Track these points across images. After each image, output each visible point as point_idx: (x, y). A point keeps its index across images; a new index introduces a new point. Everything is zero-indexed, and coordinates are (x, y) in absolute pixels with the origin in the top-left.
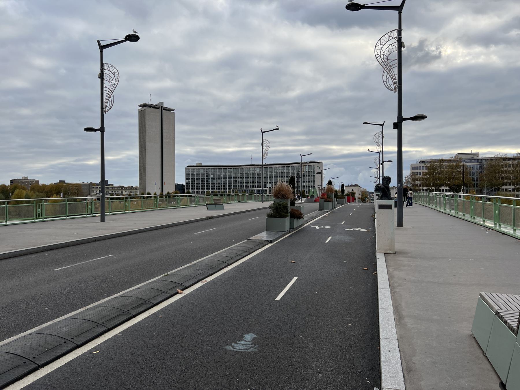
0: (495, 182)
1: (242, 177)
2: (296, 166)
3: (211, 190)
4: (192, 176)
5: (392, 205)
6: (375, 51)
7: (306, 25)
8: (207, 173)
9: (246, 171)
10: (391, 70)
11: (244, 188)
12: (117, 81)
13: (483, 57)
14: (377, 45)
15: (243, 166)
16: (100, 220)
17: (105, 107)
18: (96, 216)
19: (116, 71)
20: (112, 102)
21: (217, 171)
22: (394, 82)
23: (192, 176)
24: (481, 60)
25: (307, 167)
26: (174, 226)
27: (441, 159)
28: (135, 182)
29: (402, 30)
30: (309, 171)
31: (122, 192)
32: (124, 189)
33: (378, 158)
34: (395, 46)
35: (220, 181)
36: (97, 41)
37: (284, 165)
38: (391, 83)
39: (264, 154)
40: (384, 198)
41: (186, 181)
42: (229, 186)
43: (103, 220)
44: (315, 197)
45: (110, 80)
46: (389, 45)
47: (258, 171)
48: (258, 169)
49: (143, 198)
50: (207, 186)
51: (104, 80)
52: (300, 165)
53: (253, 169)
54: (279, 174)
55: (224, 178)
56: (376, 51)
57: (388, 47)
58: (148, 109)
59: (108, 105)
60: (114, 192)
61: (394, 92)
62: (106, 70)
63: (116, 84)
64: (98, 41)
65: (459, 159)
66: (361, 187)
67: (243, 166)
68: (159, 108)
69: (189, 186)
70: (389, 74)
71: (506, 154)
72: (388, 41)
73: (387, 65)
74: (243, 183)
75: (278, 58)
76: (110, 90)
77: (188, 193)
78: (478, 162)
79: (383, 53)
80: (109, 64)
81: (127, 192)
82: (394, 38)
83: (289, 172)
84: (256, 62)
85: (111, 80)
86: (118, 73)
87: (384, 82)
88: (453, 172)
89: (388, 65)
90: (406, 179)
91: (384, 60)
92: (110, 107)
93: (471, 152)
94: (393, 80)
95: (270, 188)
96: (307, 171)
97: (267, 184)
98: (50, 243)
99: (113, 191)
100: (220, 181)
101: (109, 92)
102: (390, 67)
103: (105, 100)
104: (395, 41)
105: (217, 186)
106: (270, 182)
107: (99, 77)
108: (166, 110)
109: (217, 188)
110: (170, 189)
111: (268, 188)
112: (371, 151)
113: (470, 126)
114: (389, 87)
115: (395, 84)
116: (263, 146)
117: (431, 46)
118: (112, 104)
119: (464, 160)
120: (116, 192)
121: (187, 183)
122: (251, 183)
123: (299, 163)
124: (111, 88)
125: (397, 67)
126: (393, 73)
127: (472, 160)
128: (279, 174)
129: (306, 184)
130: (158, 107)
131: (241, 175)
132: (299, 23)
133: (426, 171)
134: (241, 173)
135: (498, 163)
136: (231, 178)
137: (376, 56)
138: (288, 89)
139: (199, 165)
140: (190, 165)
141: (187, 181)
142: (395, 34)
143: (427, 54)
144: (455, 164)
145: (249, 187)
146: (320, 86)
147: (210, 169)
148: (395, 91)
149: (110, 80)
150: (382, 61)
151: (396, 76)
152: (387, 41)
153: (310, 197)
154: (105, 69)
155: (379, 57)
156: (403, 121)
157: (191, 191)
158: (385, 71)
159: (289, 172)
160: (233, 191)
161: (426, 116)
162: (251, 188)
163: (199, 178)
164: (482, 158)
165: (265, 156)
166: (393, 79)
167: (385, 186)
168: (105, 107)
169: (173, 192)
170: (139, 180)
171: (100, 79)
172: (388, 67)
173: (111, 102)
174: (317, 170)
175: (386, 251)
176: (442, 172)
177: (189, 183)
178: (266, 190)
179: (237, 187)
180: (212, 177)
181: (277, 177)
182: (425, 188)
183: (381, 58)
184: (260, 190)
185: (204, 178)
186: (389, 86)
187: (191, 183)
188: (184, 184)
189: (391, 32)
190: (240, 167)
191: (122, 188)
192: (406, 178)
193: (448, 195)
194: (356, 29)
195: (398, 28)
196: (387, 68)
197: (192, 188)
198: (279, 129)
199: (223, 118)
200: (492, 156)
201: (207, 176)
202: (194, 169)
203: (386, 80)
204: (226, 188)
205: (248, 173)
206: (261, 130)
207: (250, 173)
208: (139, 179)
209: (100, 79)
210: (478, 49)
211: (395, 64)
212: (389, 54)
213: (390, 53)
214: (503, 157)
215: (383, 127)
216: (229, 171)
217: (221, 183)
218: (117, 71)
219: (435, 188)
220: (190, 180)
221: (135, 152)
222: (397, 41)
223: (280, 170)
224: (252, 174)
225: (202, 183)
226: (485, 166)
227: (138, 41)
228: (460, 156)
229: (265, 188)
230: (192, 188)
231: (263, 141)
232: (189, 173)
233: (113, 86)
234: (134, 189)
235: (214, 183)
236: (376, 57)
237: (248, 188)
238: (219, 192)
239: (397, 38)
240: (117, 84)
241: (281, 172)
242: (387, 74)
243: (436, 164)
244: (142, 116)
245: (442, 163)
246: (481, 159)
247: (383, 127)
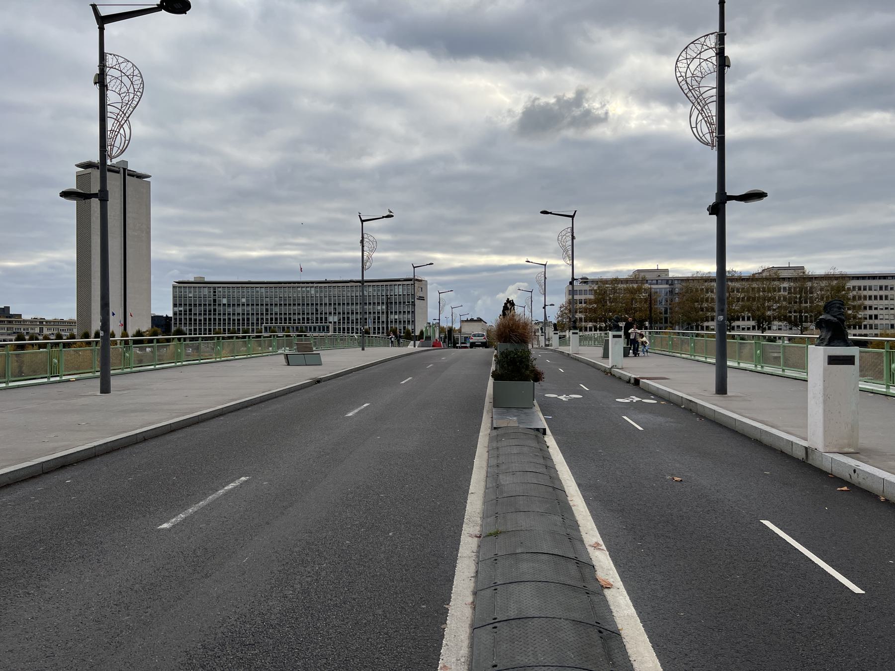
0: (693, 315)
1: (282, 303)
2: (381, 285)
4: (185, 300)
5: (854, 356)
6: (676, 70)
7: (394, 48)
10: (706, 107)
12: (139, 94)
13: (667, 121)
14: (680, 59)
16: (99, 389)
17: (109, 147)
18: (69, 381)
19: (136, 72)
20: (127, 138)
21: (234, 292)
22: (711, 130)
23: (185, 300)
24: (665, 126)
25: (401, 287)
27: (615, 279)
28: (67, 310)
29: (725, 34)
30: (403, 295)
31: (41, 330)
32: (44, 325)
33: (543, 273)
34: (712, 63)
35: (239, 310)
36: (91, 5)
38: (705, 130)
39: (365, 262)
40: (836, 342)
42: (258, 320)
43: (105, 389)
44: (433, 340)
45: (123, 91)
46: (702, 60)
47: (313, 292)
48: (313, 289)
49: (157, 343)
50: (215, 319)
51: (107, 90)
52: (412, 282)
53: (304, 289)
54: (352, 299)
55: (249, 305)
56: (677, 71)
57: (700, 63)
59: (117, 144)
60: (24, 330)
61: (710, 147)
62: (112, 67)
63: (137, 100)
64: (94, 7)
65: (642, 278)
66: (486, 323)
68: (118, 172)
69: (189, 318)
70: (702, 114)
71: (709, 273)
72: (700, 53)
73: (698, 97)
74: (285, 314)
75: (345, 99)
76: (121, 113)
77: (179, 332)
78: (667, 284)
79: (691, 75)
80: (118, 56)
81: (52, 329)
82: (712, 48)
83: (369, 296)
84: (305, 103)
85: (124, 90)
86: (141, 77)
87: (692, 128)
88: (633, 299)
89: (701, 97)
90: (562, 309)
91: (692, 87)
92: (121, 148)
94: (708, 124)
95: (335, 323)
96: (400, 294)
97: (330, 317)
98: (55, 450)
99: (22, 327)
100: (239, 310)
101: (119, 117)
102: (703, 102)
103: (109, 132)
104: (712, 53)
105: (234, 320)
106: (335, 313)
107: (95, 83)
108: (132, 176)
109: (234, 324)
110: (140, 323)
111: (331, 323)
112: (532, 262)
113: (647, 228)
114: (701, 138)
115: (712, 132)
116: (363, 246)
117: (594, 101)
118: (127, 142)
119: (647, 280)
120: (28, 329)
121: (177, 314)
122: (200, 314)
123: (410, 280)
124: (124, 108)
125: (716, 101)
126: (709, 112)
127: (659, 281)
128: (352, 299)
129: (409, 317)
130: (117, 169)
131: (280, 300)
132: (382, 43)
133: (592, 297)
134: (281, 296)
135: (696, 285)
136: (200, 305)
137: (677, 79)
138: (362, 152)
139: (198, 280)
140: (181, 280)
141: (176, 309)
142: (712, 41)
143: (588, 113)
144: (635, 286)
146: (416, 152)
147: (308, 287)
148: (713, 146)
149: (123, 91)
150: (689, 88)
151: (714, 118)
152: (699, 52)
153: (425, 340)
154: (110, 66)
155: (684, 82)
156: (727, 202)
157: (183, 328)
158: (694, 107)
159: (369, 296)
160: (266, 328)
161: (767, 193)
162: (300, 323)
163: (200, 305)
164: (674, 278)
165: (368, 264)
166: (709, 124)
168: (109, 147)
169: (147, 331)
170: (77, 307)
171: (96, 88)
172: (699, 101)
173: (125, 138)
174: (419, 294)
175: (842, 448)
176: (614, 300)
177: (180, 314)
178: (328, 327)
179: (274, 322)
180: (224, 303)
181: (348, 304)
182: (590, 325)
183: (687, 83)
184: (316, 327)
185: (210, 305)
186: (701, 135)
187: (184, 314)
188: (171, 314)
189: (706, 36)
190: (280, 285)
191: (42, 322)
192: (561, 308)
194: (476, 62)
195: (718, 31)
196: (698, 103)
197: (185, 324)
198: (392, 216)
199: (243, 196)
200: (689, 275)
201: (215, 301)
203: (697, 124)
204: (253, 323)
205: (294, 296)
206: (360, 216)
207: (298, 297)
208: (77, 305)
209: (98, 87)
210: (660, 109)
211: (713, 96)
212: (702, 78)
213: (703, 76)
214: (706, 277)
215: (573, 220)
216: (257, 292)
217: (344, 313)
218: (138, 72)
219: (606, 324)
220: (182, 309)
221: (71, 254)
222: (717, 54)
223: (353, 291)
224: (301, 298)
225: (205, 314)
226: (677, 291)
227: (186, 13)
228: (642, 274)
229: (327, 323)
230: (185, 324)
231: (363, 237)
233: (129, 103)
234: (66, 324)
235: (229, 314)
236: (678, 82)
237: (294, 323)
238: (253, 331)
239: (716, 48)
240: (139, 100)
241: (356, 296)
242: (699, 114)
243: (607, 286)
245: (616, 285)
246: (672, 279)
247: (574, 220)
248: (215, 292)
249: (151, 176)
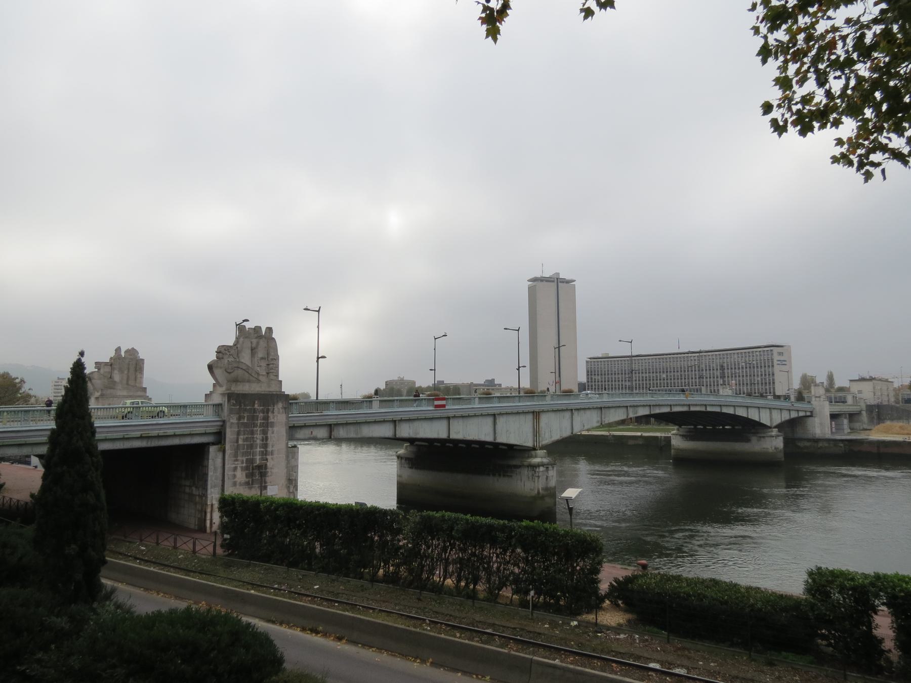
15: (666, 355)
26: (469, 416)
37: (726, 352)
58: (539, 284)
67: (666, 355)
68: (553, 281)
93: (630, 354)
108: (563, 282)
129: (758, 379)
139: (604, 356)
202: (727, 354)
209: (769, 43)
244: (532, 292)
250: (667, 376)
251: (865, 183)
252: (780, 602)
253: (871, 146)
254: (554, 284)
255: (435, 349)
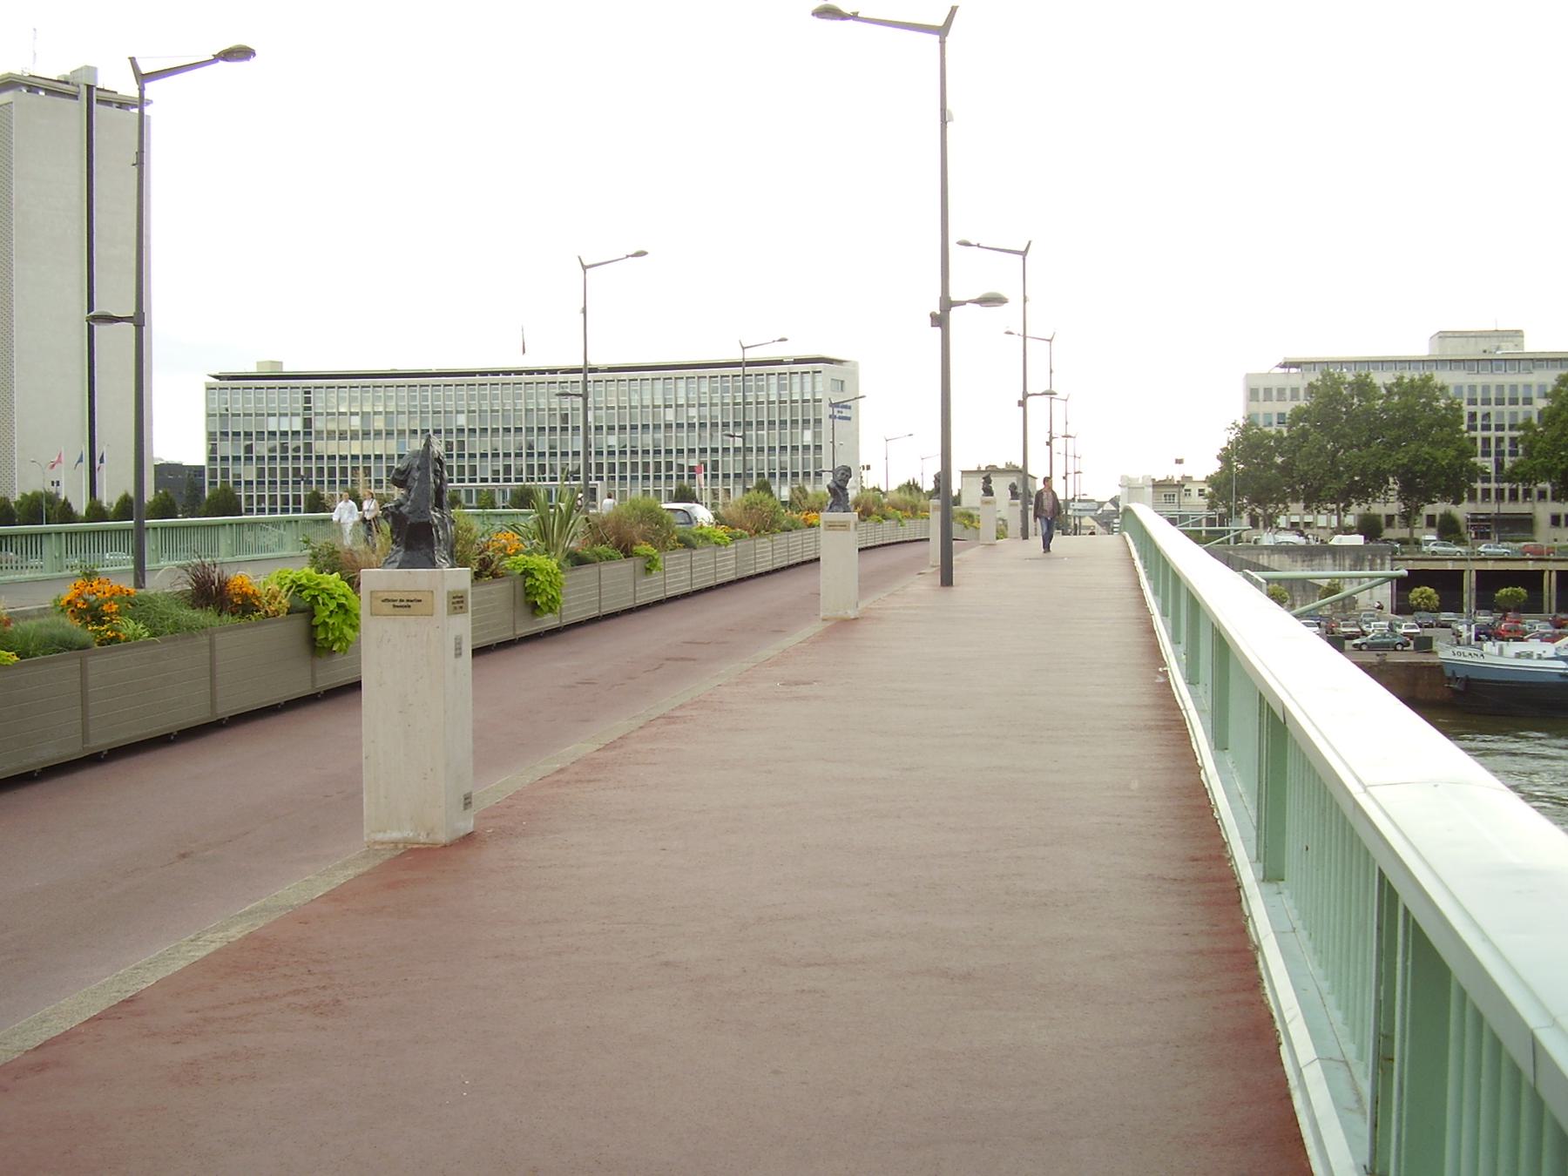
3: (246, 490)
8: (310, 408)
9: (504, 399)
11: (463, 481)
25: (773, 380)
30: (780, 402)
41: (1247, 407)
68: (75, 97)
108: (108, 103)
129: (783, 458)
139: (266, 371)
141: (1255, 407)
145: (524, 476)
167: (838, 486)
193: (1177, 517)
207: (550, 409)
215: (942, 43)
232: (421, 406)
247: (948, 45)
248: (308, 400)
249: (958, 243)
250: (261, 472)
251: (957, 7)
252: (1334, 519)
253: (1554, 406)
254: (78, 108)
255: (584, 311)
